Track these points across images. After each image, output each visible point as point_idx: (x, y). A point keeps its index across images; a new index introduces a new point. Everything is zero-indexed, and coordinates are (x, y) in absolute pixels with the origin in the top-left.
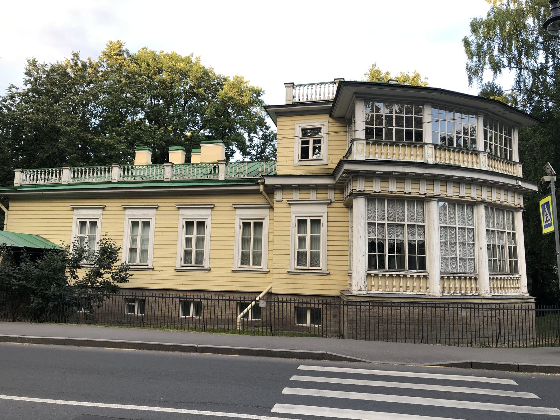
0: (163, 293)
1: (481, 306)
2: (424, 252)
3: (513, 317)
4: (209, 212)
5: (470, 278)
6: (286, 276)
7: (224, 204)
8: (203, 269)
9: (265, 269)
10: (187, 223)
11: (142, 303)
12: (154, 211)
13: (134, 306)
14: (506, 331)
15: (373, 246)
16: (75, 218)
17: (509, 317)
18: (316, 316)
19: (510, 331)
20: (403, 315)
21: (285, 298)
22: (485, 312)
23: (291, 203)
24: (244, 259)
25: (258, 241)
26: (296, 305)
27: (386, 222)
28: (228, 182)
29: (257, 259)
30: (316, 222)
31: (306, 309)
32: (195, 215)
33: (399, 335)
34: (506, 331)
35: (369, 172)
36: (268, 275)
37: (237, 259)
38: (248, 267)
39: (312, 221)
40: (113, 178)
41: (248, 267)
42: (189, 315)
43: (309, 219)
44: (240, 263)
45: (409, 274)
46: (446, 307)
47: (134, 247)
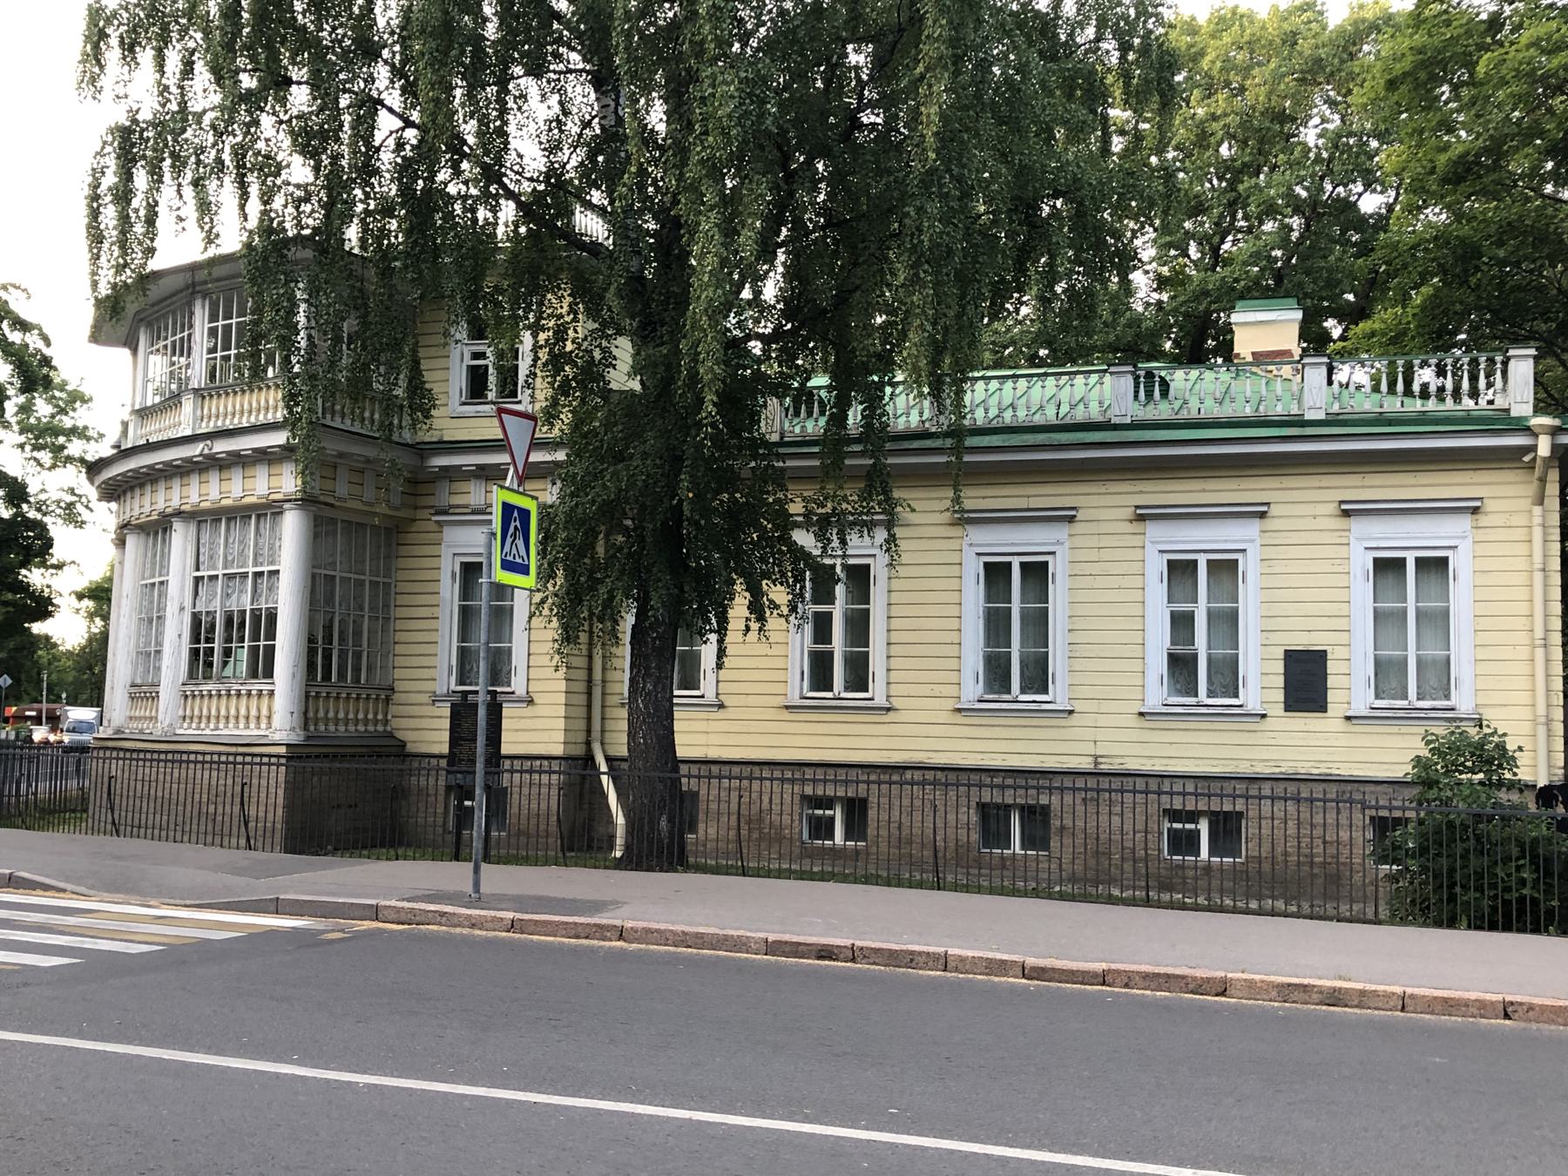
0: (1102, 783)
2: (195, 653)
3: (190, 786)
4: (1059, 533)
7: (1104, 505)
8: (869, 703)
9: (880, 700)
10: (1172, 565)
11: (856, 811)
12: (1465, 522)
13: (832, 819)
14: (173, 817)
17: (182, 786)
19: (180, 819)
22: (199, 766)
23: (964, 519)
25: (1437, 621)
26: (1373, 813)
27: (367, 578)
30: (1434, 567)
31: (1008, 808)
32: (1410, 537)
33: (156, 832)
34: (173, 817)
37: (446, 667)
41: (1403, 703)
42: (832, 838)
43: (1016, 562)
44: (453, 678)
46: (1383, 807)
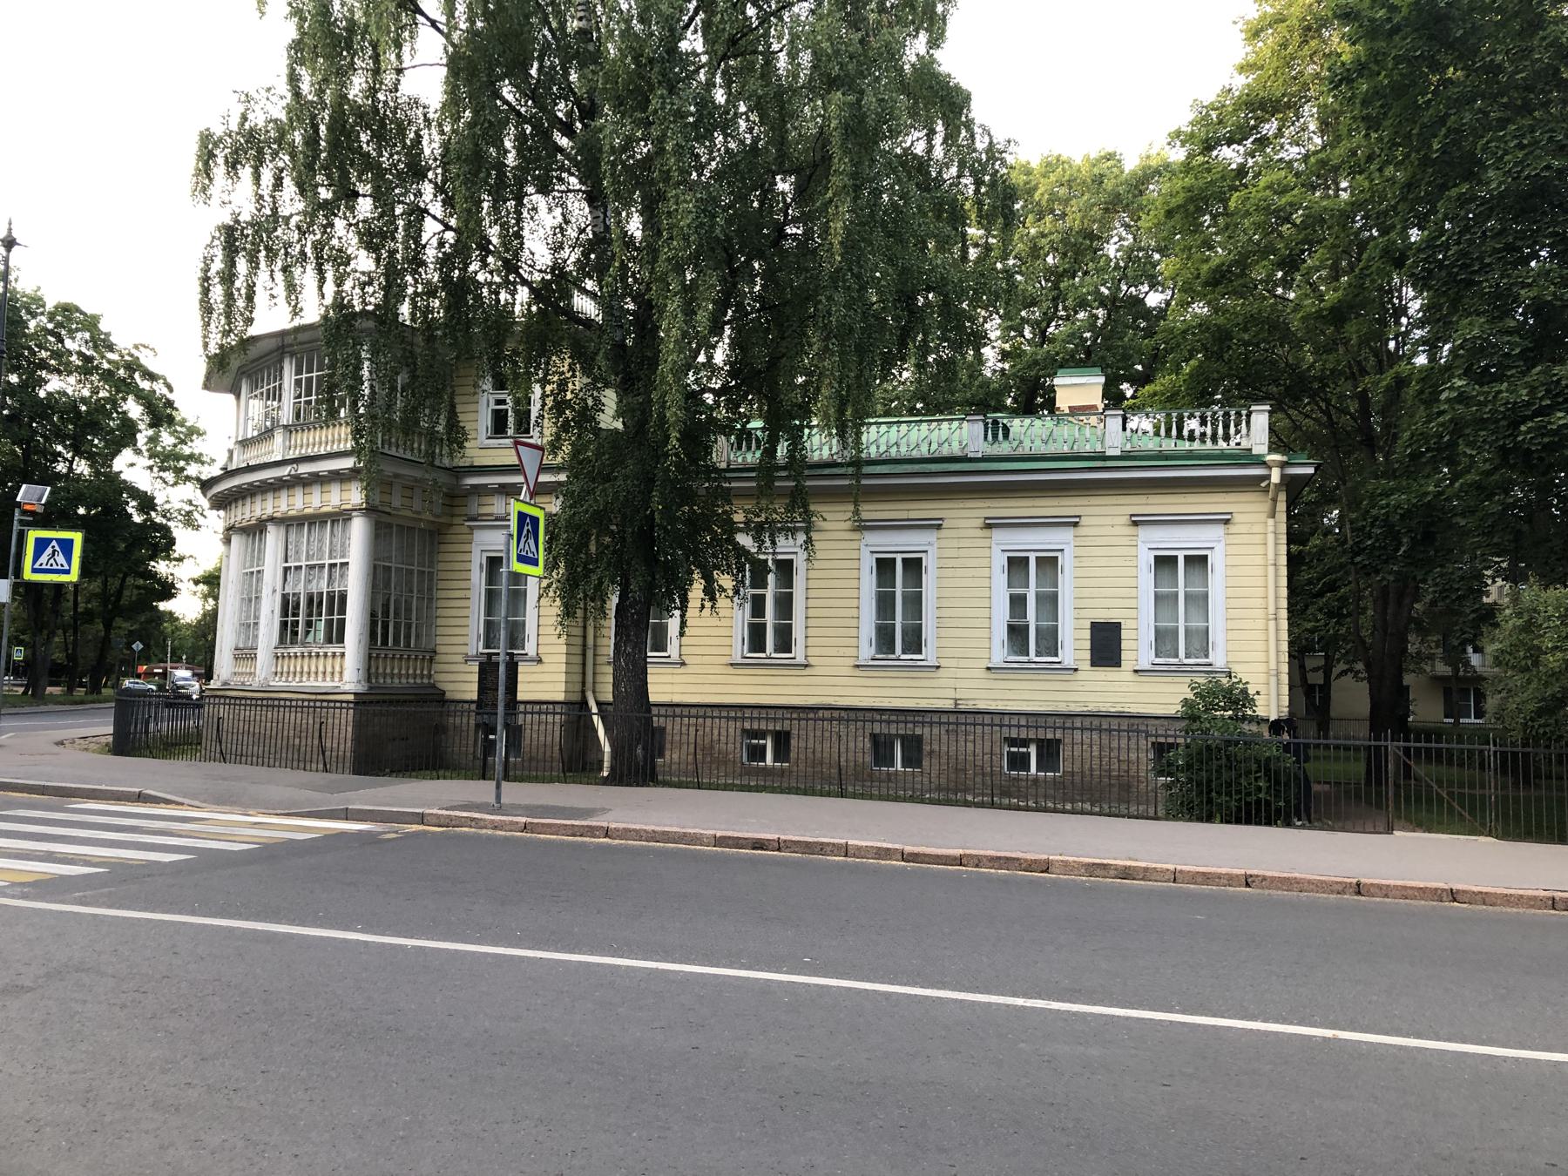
0: (961, 718)
1: (936, 719)
5: (318, 655)
6: (984, 674)
9: (800, 659)
15: (288, 606)
16: (996, 550)
18: (914, 754)
20: (1087, 755)
21: (827, 714)
23: (861, 526)
24: (885, 639)
25: (1199, 601)
27: (415, 568)
28: (1167, 458)
29: (914, 642)
30: (1198, 562)
32: (1181, 541)
35: (502, 486)
36: (808, 671)
38: (1025, 659)
39: (1189, 560)
40: (1108, 443)
43: (1032, 557)
45: (322, 652)
47: (1020, 622)
